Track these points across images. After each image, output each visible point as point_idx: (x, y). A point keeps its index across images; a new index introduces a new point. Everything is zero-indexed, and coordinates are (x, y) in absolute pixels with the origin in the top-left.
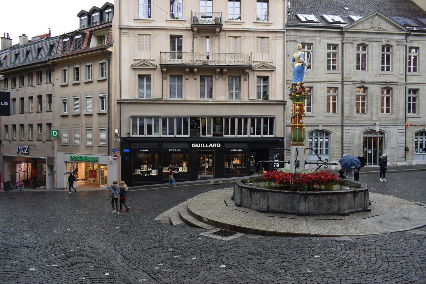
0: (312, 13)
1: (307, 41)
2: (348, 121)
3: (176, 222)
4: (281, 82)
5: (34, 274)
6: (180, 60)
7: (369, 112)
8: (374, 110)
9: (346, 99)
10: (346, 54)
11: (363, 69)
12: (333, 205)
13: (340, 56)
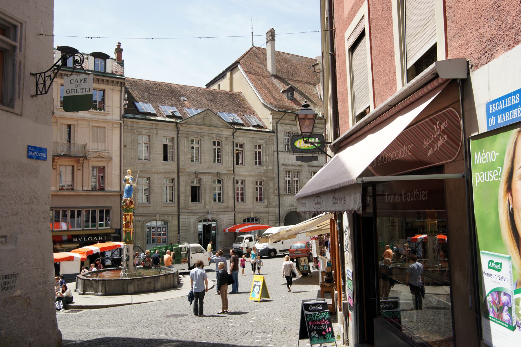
2: (183, 211)
4: (118, 172)
7: (203, 201)
8: (207, 199)
9: (182, 189)
10: (181, 147)
12: (151, 285)
13: (176, 148)
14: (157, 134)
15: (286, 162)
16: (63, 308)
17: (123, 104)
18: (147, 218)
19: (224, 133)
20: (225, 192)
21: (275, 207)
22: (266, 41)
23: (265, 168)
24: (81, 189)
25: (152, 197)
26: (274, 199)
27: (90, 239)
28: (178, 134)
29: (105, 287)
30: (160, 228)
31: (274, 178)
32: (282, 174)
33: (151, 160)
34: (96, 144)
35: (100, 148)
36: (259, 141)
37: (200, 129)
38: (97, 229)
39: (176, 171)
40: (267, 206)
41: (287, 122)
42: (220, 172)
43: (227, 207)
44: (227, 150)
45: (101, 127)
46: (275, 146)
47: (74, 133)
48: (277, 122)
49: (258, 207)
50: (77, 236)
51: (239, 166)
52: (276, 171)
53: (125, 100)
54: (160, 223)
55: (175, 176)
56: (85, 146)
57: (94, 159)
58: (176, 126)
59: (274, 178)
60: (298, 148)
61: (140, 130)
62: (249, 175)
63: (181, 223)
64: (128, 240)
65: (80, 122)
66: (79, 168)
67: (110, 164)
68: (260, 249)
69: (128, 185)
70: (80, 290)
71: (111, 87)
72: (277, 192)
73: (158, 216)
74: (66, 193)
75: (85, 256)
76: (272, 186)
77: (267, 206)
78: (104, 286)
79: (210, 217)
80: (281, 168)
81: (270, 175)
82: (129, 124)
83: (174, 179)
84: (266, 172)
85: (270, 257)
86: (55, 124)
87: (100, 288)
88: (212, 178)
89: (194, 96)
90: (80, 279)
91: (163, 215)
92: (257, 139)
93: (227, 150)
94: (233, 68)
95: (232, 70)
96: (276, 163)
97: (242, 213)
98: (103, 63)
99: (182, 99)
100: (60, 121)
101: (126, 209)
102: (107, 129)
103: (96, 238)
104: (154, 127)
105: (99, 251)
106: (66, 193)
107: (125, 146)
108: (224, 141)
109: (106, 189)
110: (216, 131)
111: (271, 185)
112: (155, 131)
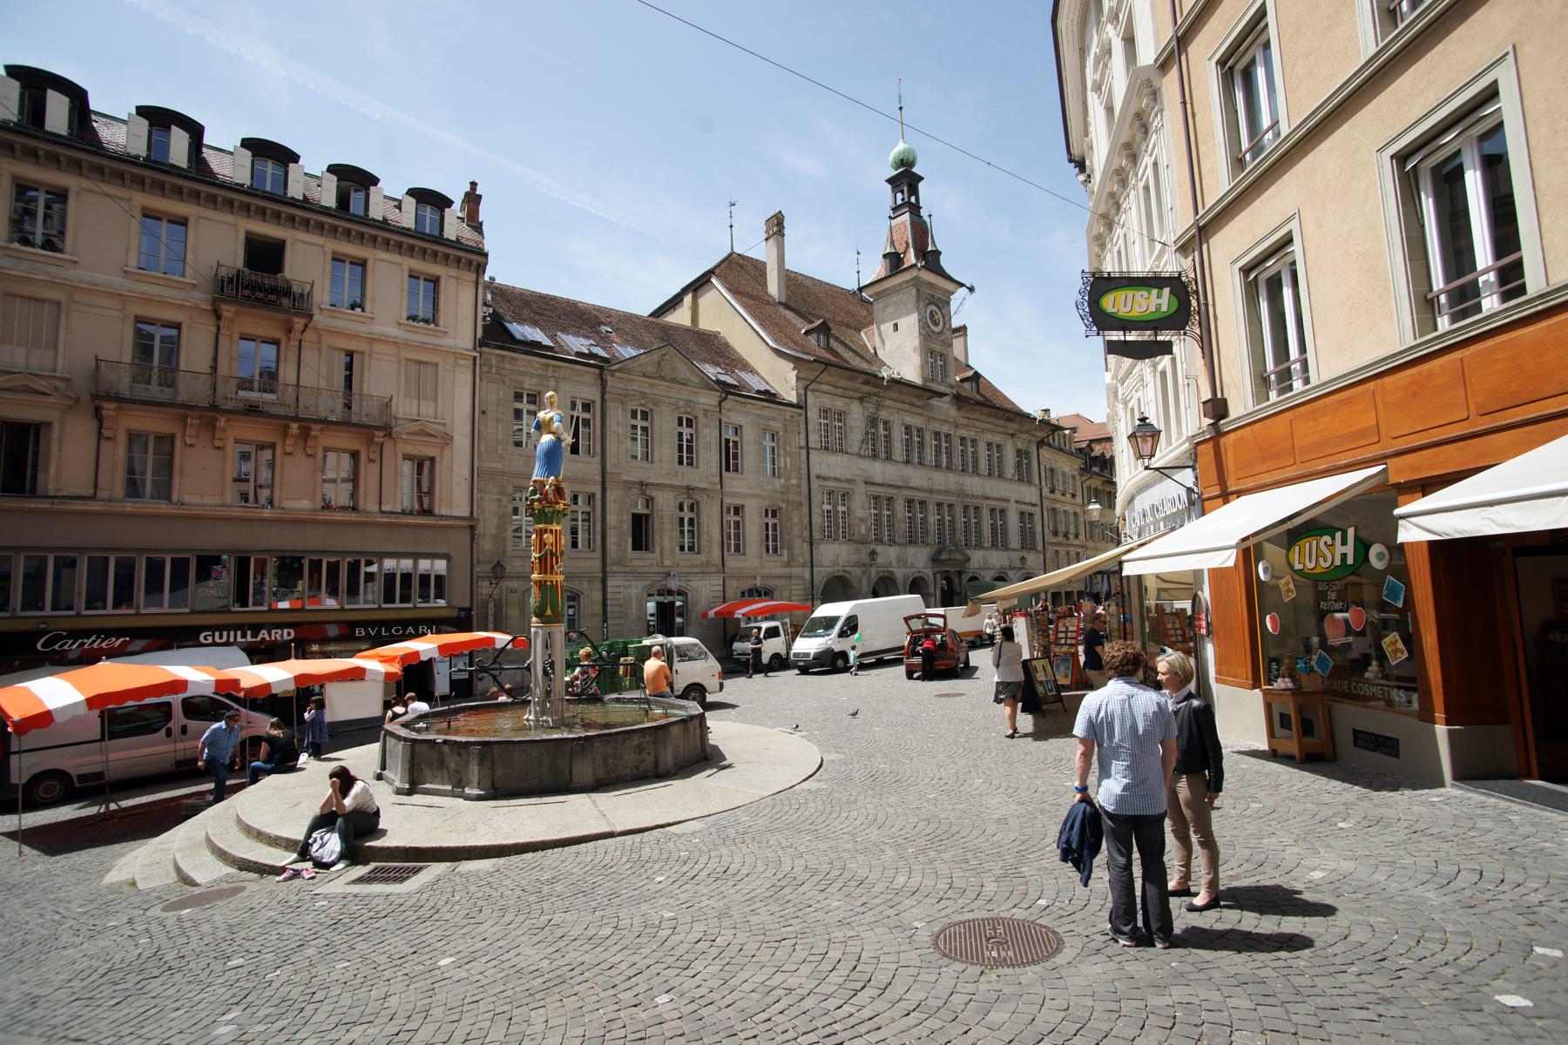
0: (535, 324)
1: (529, 384)
2: (615, 568)
3: (208, 871)
4: (466, 472)
5: (764, 959)
6: (168, 391)
7: (657, 549)
8: (667, 544)
9: (612, 518)
10: (612, 424)
11: (690, 464)
12: (644, 755)
13: (598, 425)
15: (824, 471)
16: (342, 856)
17: (480, 315)
19: (702, 400)
20: (704, 530)
21: (803, 566)
26: (801, 549)
28: (603, 393)
29: (492, 769)
31: (800, 504)
35: (423, 410)
37: (652, 386)
40: (788, 565)
41: (824, 387)
42: (694, 484)
44: (708, 437)
45: (426, 363)
46: (803, 436)
48: (806, 385)
50: (364, 624)
51: (732, 474)
52: (805, 490)
53: (485, 304)
55: (597, 490)
56: (388, 405)
58: (601, 375)
59: (800, 504)
61: (520, 378)
64: (549, 612)
65: (377, 347)
67: (447, 451)
68: (812, 652)
69: (547, 438)
70: (396, 776)
71: (453, 272)
72: (806, 534)
74: (338, 516)
75: (396, 668)
76: (797, 519)
77: (788, 565)
78: (487, 764)
79: (673, 584)
80: (815, 484)
81: (793, 497)
84: (786, 490)
85: (835, 670)
87: (474, 771)
89: (628, 327)
90: (399, 738)
92: (767, 418)
93: (708, 437)
94: (698, 286)
95: (695, 290)
96: (804, 472)
97: (738, 577)
99: (604, 328)
100: (328, 340)
103: (411, 630)
106: (338, 516)
108: (701, 416)
109: (436, 512)
110: (683, 394)
111: (796, 520)
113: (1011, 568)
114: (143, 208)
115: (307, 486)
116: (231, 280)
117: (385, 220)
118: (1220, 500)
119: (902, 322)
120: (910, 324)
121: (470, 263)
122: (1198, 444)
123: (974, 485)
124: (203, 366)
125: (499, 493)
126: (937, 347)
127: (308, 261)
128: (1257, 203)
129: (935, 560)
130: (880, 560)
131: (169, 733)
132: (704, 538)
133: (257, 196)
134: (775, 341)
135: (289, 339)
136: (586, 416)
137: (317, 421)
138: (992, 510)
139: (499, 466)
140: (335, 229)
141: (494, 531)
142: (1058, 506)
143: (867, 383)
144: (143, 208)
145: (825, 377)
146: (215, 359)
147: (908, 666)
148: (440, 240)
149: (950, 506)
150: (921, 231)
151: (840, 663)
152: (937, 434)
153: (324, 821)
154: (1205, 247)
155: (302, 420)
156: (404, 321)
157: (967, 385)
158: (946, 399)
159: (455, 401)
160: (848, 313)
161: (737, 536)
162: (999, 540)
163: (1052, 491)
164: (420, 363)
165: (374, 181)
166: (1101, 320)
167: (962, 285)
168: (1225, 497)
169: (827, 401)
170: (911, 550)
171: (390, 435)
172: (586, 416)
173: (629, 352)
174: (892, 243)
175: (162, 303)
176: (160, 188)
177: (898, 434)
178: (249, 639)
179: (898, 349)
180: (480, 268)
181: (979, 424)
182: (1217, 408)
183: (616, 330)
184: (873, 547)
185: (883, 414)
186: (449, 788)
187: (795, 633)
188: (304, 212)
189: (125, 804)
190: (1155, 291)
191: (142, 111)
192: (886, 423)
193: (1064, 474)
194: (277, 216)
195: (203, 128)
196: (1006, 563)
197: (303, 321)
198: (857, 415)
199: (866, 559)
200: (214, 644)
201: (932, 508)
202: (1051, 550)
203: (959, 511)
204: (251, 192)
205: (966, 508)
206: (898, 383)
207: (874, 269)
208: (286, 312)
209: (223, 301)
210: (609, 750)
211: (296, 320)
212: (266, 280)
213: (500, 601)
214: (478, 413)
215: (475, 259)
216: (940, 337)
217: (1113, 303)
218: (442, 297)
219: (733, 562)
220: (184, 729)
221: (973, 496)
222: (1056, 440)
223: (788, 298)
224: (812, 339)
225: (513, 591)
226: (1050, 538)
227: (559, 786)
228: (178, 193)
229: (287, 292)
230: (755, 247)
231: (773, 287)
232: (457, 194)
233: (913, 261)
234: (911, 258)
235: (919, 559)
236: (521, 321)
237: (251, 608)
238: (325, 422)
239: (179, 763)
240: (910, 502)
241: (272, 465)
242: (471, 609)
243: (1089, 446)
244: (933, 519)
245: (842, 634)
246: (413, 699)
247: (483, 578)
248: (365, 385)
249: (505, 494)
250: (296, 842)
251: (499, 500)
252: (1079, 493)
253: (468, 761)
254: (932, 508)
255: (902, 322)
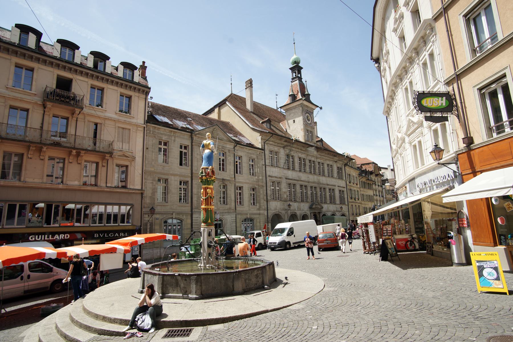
0: (164, 116)
1: (164, 138)
2: (196, 210)
4: (140, 172)
11: (223, 170)
12: (259, 279)
13: (190, 155)
14: (174, 141)
15: (271, 174)
16: (152, 326)
17: (147, 111)
18: (165, 216)
19: (228, 146)
20: (229, 196)
21: (264, 210)
22: (245, 87)
23: (257, 177)
24: (105, 185)
25: (169, 197)
26: (263, 203)
27: (111, 235)
28: (192, 143)
29: (201, 286)
30: (175, 226)
32: (269, 184)
33: (170, 164)
34: (121, 143)
35: (124, 147)
36: (252, 155)
38: (119, 225)
39: (190, 175)
40: (259, 209)
41: (271, 143)
42: (225, 178)
43: (230, 208)
46: (264, 160)
47: (101, 131)
48: (265, 142)
49: (252, 209)
54: (175, 221)
55: (189, 179)
56: (111, 144)
57: (119, 157)
60: (425, 107)
62: (246, 183)
63: (194, 221)
64: (209, 221)
65: (107, 122)
66: (104, 164)
68: (277, 242)
69: (207, 151)
71: (137, 94)
72: (265, 197)
73: (174, 214)
74: (89, 188)
76: (262, 192)
77: (259, 209)
78: (199, 284)
80: (268, 179)
81: (260, 184)
82: (151, 129)
83: (188, 181)
84: (258, 181)
86: (83, 120)
87: (193, 287)
88: (218, 183)
89: (197, 119)
91: (178, 213)
92: (251, 154)
93: (230, 160)
94: (221, 105)
95: (219, 107)
96: (264, 174)
97: (241, 214)
98: (131, 73)
100: (88, 118)
101: (206, 180)
102: (131, 131)
103: (117, 234)
104: (172, 134)
105: (144, 242)
106: (89, 188)
107: (147, 148)
109: (128, 187)
111: (261, 192)
112: (173, 138)
113: (337, 211)
114: (16, 63)
115: (77, 175)
116: (51, 93)
117: (111, 73)
118: (472, 175)
119: (297, 120)
120: (300, 120)
121: (143, 91)
122: (458, 154)
123: (324, 180)
124: (38, 125)
125: (153, 180)
126: (309, 129)
127: (81, 87)
128: (486, 64)
129: (311, 208)
130: (292, 208)
131: (22, 278)
132: (229, 199)
133: (63, 61)
134: (253, 125)
135: (73, 117)
136: (185, 151)
137: (83, 150)
138: (330, 189)
139: (153, 169)
140: (92, 76)
141: (150, 195)
142: (352, 188)
143: (286, 141)
144: (16, 63)
145: (272, 139)
146: (42, 124)
147: (319, 246)
148: (132, 82)
149: (315, 188)
150: (303, 87)
151: (288, 246)
152: (310, 161)
153: (142, 309)
154: (459, 82)
155: (77, 149)
156: (118, 112)
157: (318, 143)
158: (313, 148)
159: (136, 144)
160: (274, 116)
161: (240, 198)
162: (332, 201)
163: (350, 183)
164: (123, 128)
165: (108, 58)
166: (422, 108)
167: (318, 107)
168: (475, 173)
169: (272, 148)
170: (302, 204)
171: (111, 156)
172: (185, 151)
173: (200, 128)
174: (292, 91)
175: (21, 100)
176: (24, 56)
177: (297, 160)
178: (50, 238)
179: (295, 129)
180: (147, 93)
181: (324, 157)
182: (469, 140)
183: (193, 120)
184: (289, 203)
185: (292, 153)
186: (181, 295)
187: (268, 234)
188: (81, 69)
189: (8, 309)
190: (440, 98)
191: (17, 26)
192: (292, 156)
193: (353, 176)
194: (70, 69)
195: (42, 34)
196: (335, 209)
197: (79, 110)
198: (282, 153)
199: (287, 207)
200: (35, 240)
201: (309, 188)
202: (350, 204)
203: (318, 190)
204: (60, 59)
205: (321, 188)
206: (297, 141)
207: (286, 100)
208: (73, 106)
209: (48, 101)
210: (247, 277)
211: (76, 109)
212: (65, 93)
213: (152, 223)
214: (145, 149)
215: (145, 90)
216: (310, 126)
217: (427, 102)
218: (133, 104)
219: (239, 208)
220: (29, 277)
221: (323, 184)
222: (350, 164)
223: (254, 110)
224: (265, 125)
225: (157, 219)
226: (350, 200)
227: (228, 292)
228: (31, 58)
229: (74, 99)
230: (241, 92)
231: (249, 106)
232: (138, 65)
233: (301, 98)
234: (299, 96)
235: (305, 207)
236: (159, 115)
237: (52, 225)
238: (86, 150)
239: (25, 292)
240: (301, 186)
241: (63, 169)
242: (141, 226)
243: (361, 166)
244: (309, 192)
245: (288, 235)
246: (140, 260)
247: (146, 214)
248: (102, 136)
249: (155, 181)
250: (129, 321)
251: (152, 183)
252: (358, 183)
253: (190, 283)
254: (309, 188)
255: (297, 120)
